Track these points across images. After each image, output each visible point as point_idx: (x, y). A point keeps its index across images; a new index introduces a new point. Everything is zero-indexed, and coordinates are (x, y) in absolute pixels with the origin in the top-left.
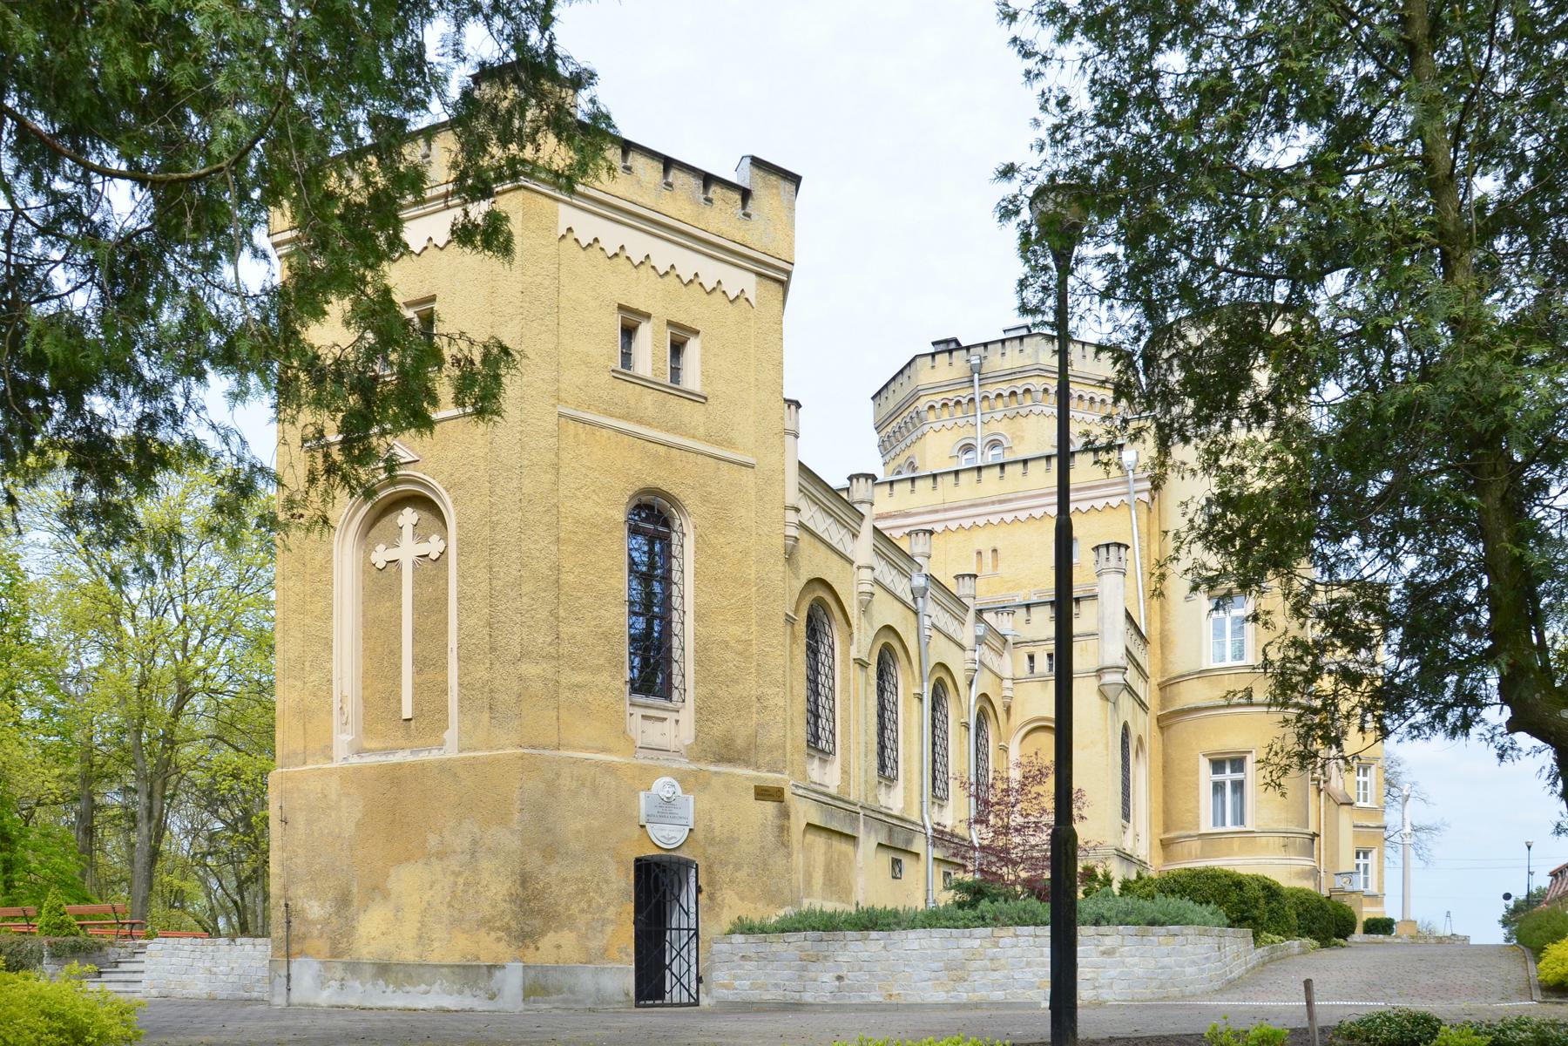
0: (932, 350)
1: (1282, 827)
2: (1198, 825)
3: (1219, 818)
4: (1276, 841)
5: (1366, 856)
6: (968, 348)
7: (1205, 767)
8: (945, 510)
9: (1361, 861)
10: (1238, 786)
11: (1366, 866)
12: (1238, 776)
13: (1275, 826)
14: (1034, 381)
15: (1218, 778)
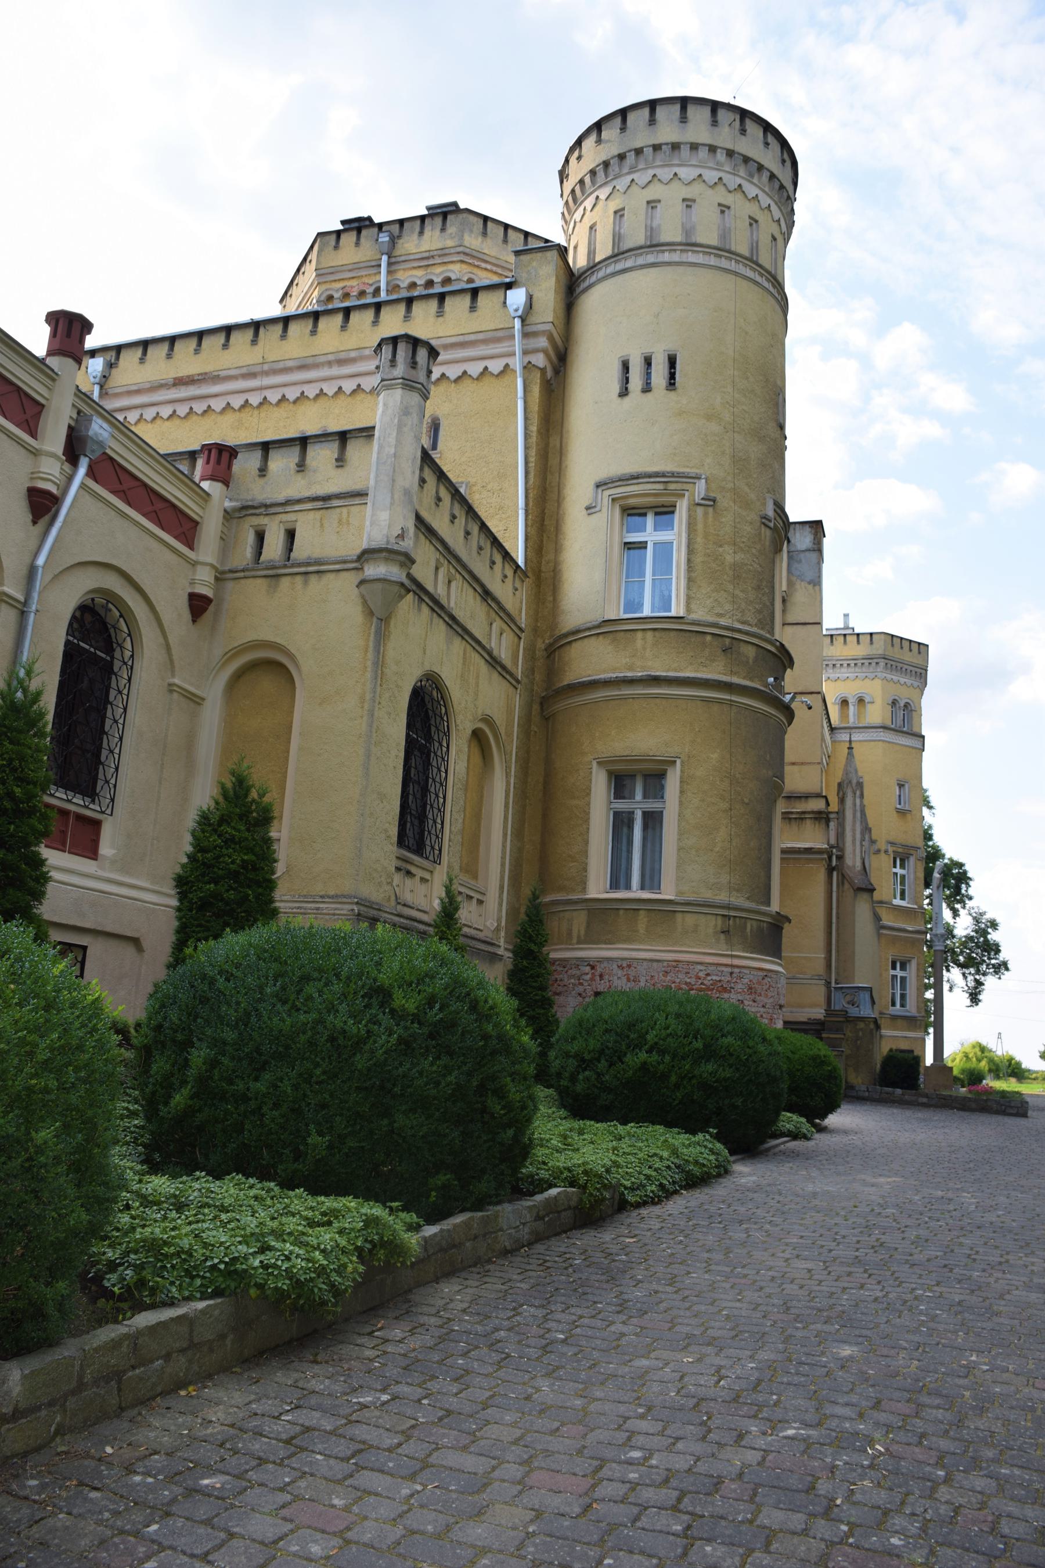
0: (341, 227)
1: (723, 897)
2: (584, 890)
3: (619, 878)
4: (709, 924)
5: (903, 967)
6: (380, 226)
7: (600, 785)
8: (266, 373)
9: (899, 973)
10: (653, 820)
11: (903, 979)
12: (652, 805)
13: (707, 895)
14: (456, 267)
15: (622, 805)
